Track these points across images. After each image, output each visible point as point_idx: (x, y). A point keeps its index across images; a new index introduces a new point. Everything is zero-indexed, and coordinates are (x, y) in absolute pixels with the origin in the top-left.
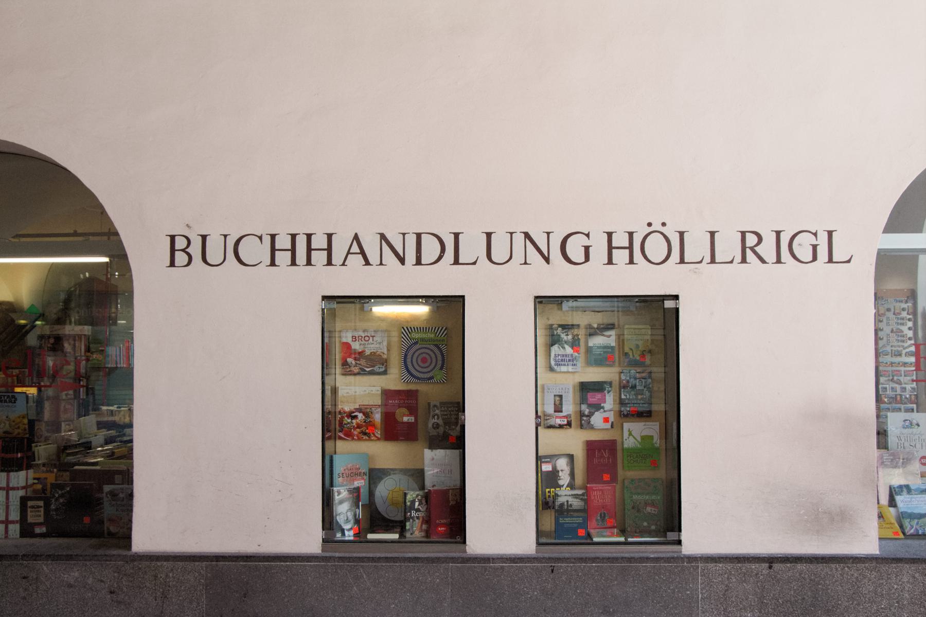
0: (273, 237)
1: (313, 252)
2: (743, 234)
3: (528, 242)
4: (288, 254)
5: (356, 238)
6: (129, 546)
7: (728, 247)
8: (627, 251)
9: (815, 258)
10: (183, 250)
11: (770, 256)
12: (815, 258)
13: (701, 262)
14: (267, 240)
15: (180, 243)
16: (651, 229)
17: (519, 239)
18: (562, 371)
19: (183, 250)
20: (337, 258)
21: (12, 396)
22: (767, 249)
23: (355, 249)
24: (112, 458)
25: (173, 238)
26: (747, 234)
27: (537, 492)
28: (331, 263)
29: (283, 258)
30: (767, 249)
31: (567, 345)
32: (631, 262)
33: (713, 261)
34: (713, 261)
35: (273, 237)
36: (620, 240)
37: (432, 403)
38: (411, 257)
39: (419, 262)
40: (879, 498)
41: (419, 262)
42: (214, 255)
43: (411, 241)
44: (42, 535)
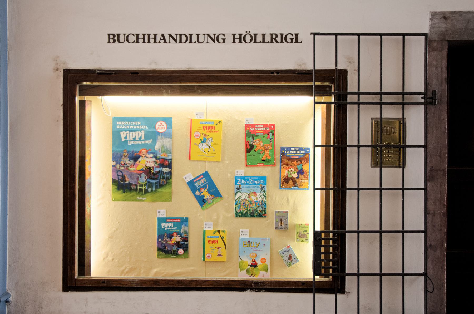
1: (239, 37)
4: (236, 37)
6: (346, 230)
7: (268, 38)
8: (338, 36)
14: (136, 36)
16: (247, 33)
17: (206, 36)
18: (282, 169)
20: (158, 41)
22: (279, 39)
23: (162, 38)
24: (123, 166)
26: (182, 35)
28: (223, 40)
29: (141, 41)
30: (279, 39)
31: (117, 180)
37: (242, 171)
38: (178, 41)
42: (121, 40)
43: (178, 36)
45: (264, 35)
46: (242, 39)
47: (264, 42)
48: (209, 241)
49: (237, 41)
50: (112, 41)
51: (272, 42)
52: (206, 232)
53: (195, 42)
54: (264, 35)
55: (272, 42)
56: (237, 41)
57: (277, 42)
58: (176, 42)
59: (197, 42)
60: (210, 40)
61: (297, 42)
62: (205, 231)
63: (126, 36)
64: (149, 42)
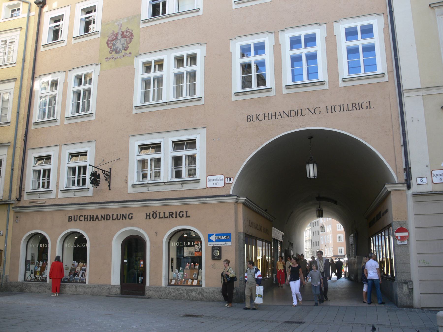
0: (264, 114)
2: (352, 104)
3: (284, 114)
5: (280, 113)
9: (367, 108)
10: (355, 107)
11: (358, 108)
12: (367, 108)
13: (263, 120)
15: (354, 105)
17: (307, 110)
19: (355, 107)
21: (147, 174)
25: (248, 116)
27: (10, 209)
32: (332, 112)
33: (348, 110)
34: (348, 110)
35: (264, 114)
36: (329, 108)
38: (290, 116)
39: (370, 108)
40: (437, 184)
41: (370, 108)
44: (264, 258)
45: (164, 213)
46: (333, 109)
47: (164, 217)
48: (158, 99)
49: (329, 111)
50: (249, 120)
51: (169, 217)
52: (84, 157)
53: (300, 116)
54: (164, 213)
55: (169, 217)
56: (329, 111)
57: (173, 217)
58: (288, 117)
59: (301, 115)
60: (310, 113)
61: (187, 217)
62: (86, 155)
63: (257, 116)
64: (120, 214)
